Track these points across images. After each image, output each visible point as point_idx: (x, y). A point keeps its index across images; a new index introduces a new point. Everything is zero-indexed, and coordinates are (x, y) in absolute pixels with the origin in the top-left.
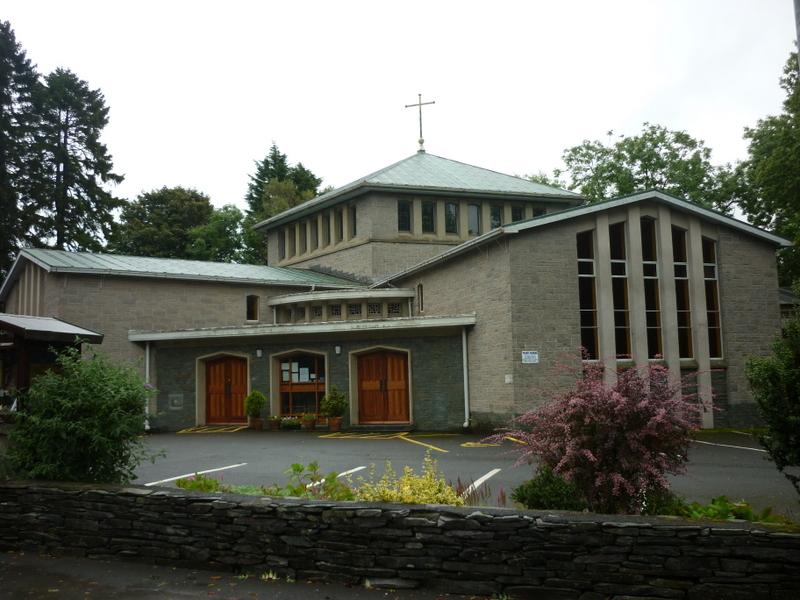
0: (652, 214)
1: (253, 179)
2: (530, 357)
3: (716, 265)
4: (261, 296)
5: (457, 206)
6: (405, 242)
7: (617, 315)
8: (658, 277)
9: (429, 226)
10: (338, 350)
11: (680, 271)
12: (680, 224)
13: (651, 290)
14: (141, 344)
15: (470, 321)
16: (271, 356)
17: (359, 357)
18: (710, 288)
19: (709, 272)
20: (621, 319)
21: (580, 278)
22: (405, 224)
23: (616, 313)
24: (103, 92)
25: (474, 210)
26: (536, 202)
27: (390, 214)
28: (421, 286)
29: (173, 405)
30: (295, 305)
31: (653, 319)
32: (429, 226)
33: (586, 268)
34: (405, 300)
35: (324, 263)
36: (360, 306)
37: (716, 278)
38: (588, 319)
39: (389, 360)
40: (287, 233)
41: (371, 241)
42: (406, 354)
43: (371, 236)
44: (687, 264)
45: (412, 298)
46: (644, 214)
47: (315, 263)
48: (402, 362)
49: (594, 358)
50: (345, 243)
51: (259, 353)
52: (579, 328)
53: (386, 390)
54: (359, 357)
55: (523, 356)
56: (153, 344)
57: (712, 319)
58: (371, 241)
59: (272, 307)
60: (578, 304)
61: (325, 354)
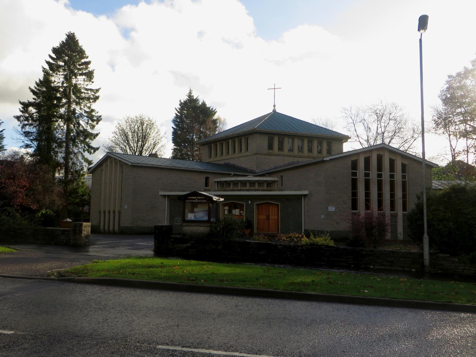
0: (381, 153)
1: (177, 110)
2: (332, 209)
3: (407, 174)
4: (211, 176)
5: (293, 139)
6: (270, 155)
7: (391, 194)
8: (383, 178)
9: (281, 148)
10: (250, 202)
11: (392, 176)
12: (393, 157)
13: (380, 184)
14: (164, 196)
15: (306, 192)
16: (255, 203)
17: (258, 205)
18: (404, 184)
19: (404, 177)
20: (367, 195)
21: (352, 178)
22: (270, 147)
23: (365, 192)
24: (437, 95)
25: (290, 140)
26: (319, 138)
27: (264, 141)
28: (282, 176)
29: (177, 222)
30: (226, 182)
31: (367, 195)
32: (281, 148)
33: (354, 174)
34: (274, 182)
35: (232, 162)
36: (255, 183)
37: (407, 180)
38: (354, 194)
39: (271, 207)
40: (213, 146)
41: (256, 154)
42: (278, 205)
43: (256, 152)
44: (370, 172)
45: (277, 181)
46: (378, 153)
47: (227, 162)
48: (276, 208)
49: (393, 211)
50: (244, 153)
51: (250, 202)
52: (351, 198)
53: (269, 219)
54: (258, 205)
55: (329, 208)
56: (168, 196)
57: (404, 196)
58: (256, 154)
59: (215, 182)
60: (351, 188)
61: (244, 203)
